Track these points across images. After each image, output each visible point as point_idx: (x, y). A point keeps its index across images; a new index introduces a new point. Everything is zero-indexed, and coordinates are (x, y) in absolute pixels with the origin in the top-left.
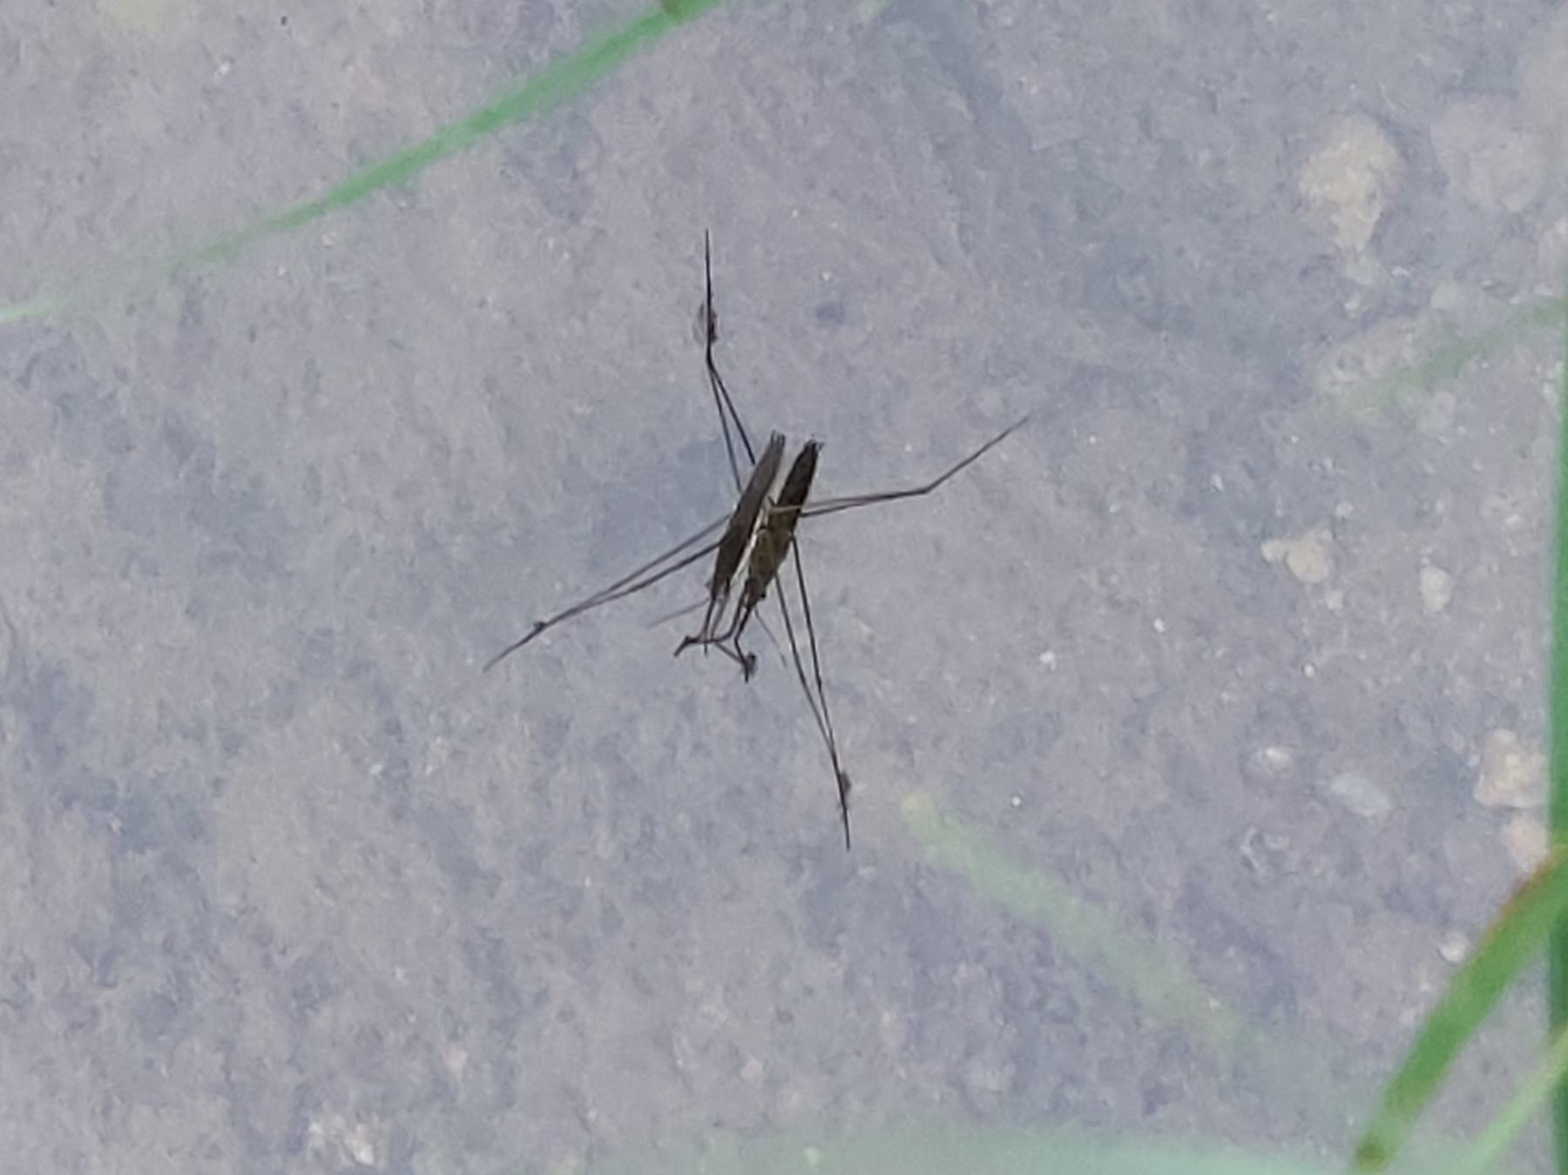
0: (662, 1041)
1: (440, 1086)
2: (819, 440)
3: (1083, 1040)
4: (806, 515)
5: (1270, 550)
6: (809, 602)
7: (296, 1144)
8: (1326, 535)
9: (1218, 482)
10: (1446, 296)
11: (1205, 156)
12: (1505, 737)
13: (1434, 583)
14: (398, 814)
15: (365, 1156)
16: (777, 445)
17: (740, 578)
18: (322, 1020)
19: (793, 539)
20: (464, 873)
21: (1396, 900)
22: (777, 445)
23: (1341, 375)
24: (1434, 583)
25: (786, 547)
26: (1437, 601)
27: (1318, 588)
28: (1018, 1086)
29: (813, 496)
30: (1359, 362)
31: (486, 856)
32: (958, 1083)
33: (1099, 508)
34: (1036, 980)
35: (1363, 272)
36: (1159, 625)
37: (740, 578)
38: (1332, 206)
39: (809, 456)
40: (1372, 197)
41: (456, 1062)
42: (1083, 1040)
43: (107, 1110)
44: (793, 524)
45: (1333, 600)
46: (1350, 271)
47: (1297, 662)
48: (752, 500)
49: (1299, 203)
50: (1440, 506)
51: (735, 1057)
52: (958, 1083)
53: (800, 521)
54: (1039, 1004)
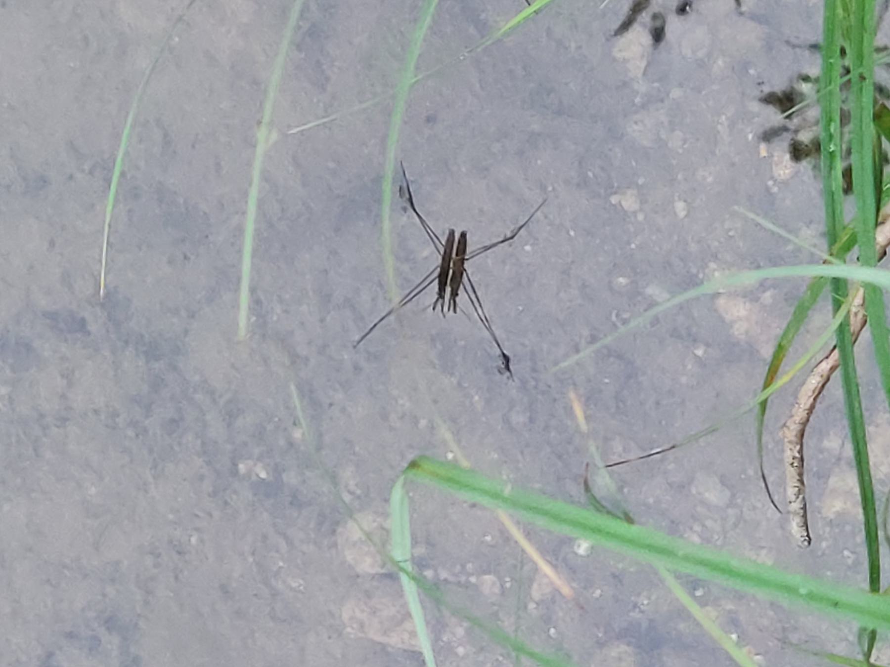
0: (385, 417)
1: (291, 444)
2: (464, 229)
3: (555, 400)
4: (467, 259)
5: (614, 200)
6: (415, 214)
7: (235, 473)
8: (635, 192)
9: (590, 174)
10: (676, 93)
11: (573, 45)
12: (712, 265)
13: (680, 207)
14: (264, 336)
15: (263, 475)
16: (452, 233)
17: (448, 289)
18: (239, 422)
19: (465, 270)
20: (295, 358)
21: (675, 334)
22: (452, 233)
23: (635, 127)
24: (680, 207)
25: (462, 274)
26: (682, 214)
27: (635, 213)
28: (531, 420)
29: (468, 250)
30: (642, 121)
31: (302, 350)
32: (506, 420)
33: (543, 188)
34: (533, 378)
35: (642, 87)
36: (572, 233)
37: (448, 289)
38: (625, 61)
39: (463, 235)
40: (643, 56)
41: (297, 434)
42: (555, 400)
43: (155, 467)
44: (463, 263)
45: (641, 217)
46: (636, 86)
47: (629, 243)
48: (446, 258)
49: (614, 60)
50: (680, 177)
51: (415, 420)
52: (506, 420)
53: (466, 262)
54: (536, 387)
